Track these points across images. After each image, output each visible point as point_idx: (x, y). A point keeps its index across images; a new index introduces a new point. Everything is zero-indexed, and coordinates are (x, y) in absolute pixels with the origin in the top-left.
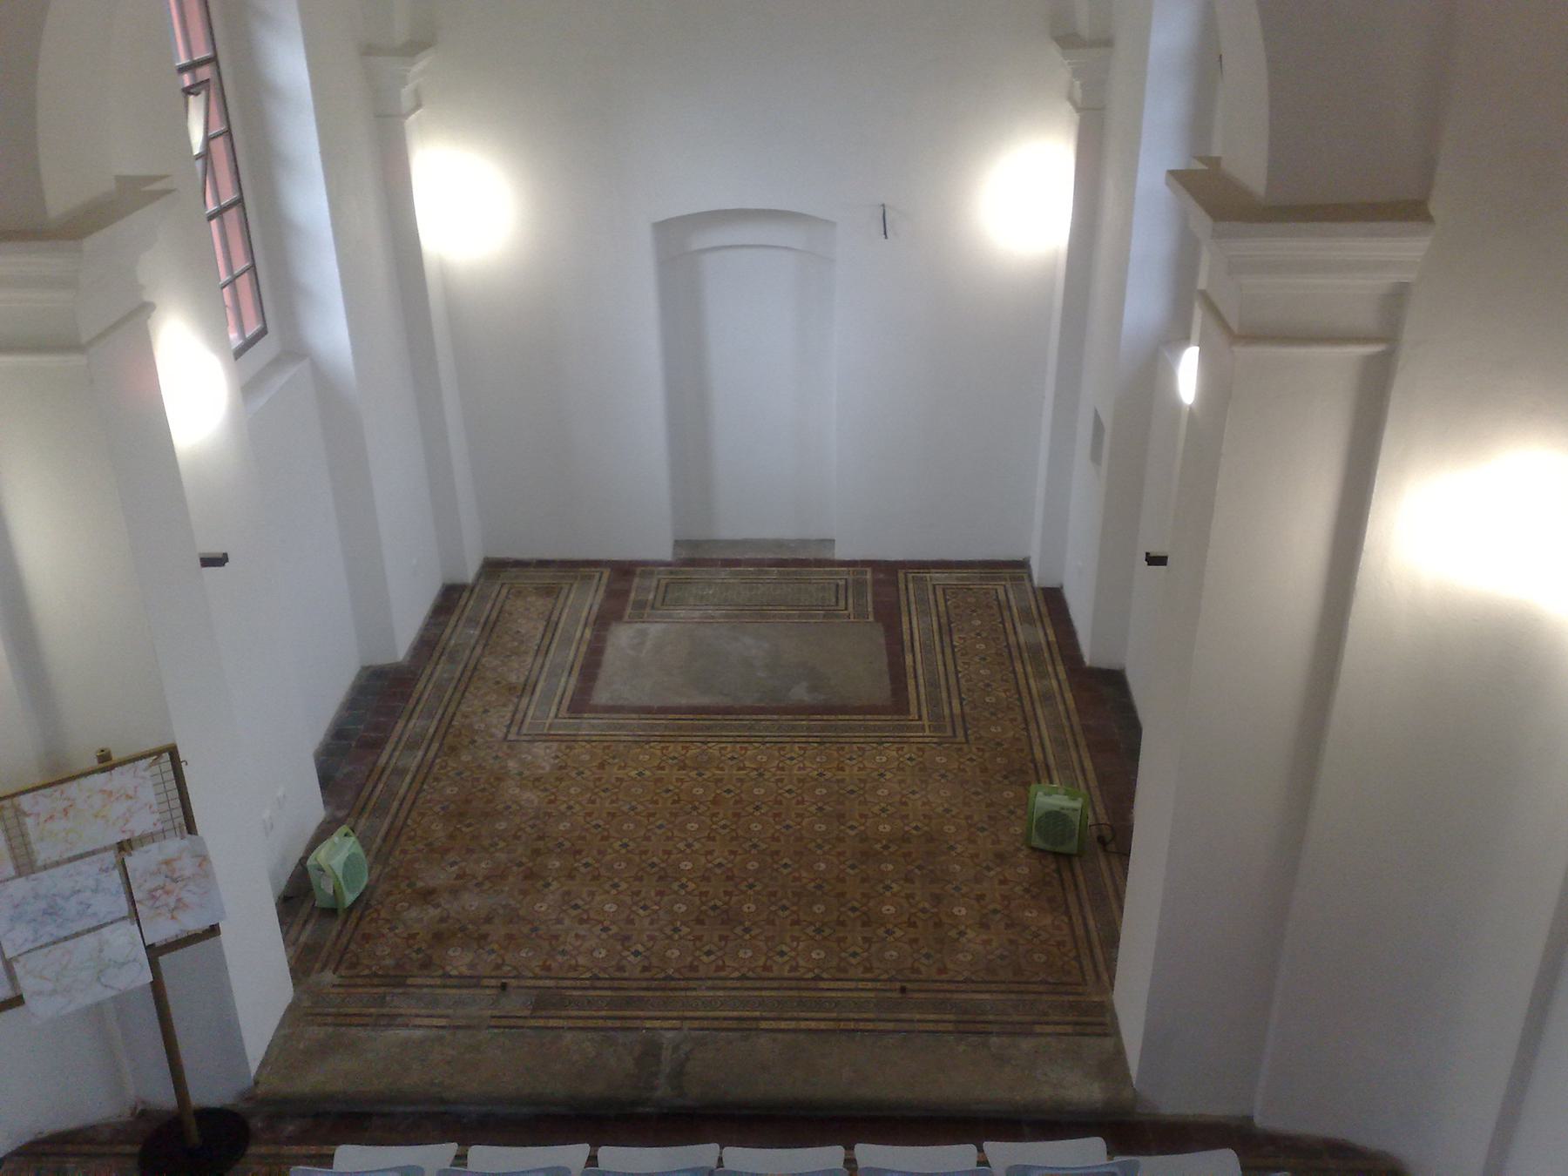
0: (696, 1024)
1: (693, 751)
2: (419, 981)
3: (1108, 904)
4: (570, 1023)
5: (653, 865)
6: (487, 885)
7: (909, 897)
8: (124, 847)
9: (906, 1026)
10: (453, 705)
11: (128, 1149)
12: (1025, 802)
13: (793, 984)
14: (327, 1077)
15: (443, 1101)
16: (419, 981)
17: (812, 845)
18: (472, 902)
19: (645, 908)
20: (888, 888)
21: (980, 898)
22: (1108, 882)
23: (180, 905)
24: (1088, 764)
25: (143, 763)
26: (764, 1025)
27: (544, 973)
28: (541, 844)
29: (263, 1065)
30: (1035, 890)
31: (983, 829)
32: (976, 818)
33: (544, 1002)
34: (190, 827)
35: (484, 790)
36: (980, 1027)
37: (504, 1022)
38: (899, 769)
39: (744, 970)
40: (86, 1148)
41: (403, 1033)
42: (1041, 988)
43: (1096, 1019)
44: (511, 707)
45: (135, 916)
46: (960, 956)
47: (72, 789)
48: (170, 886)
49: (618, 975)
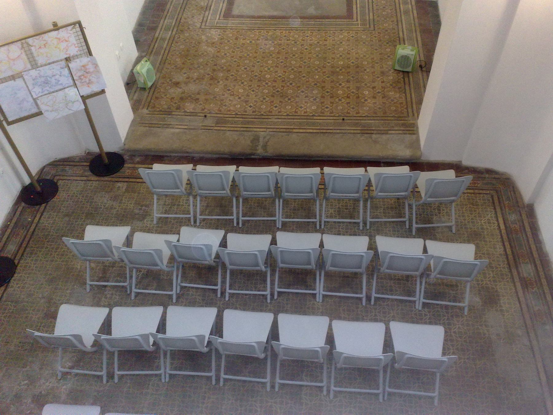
0: (271, 130)
1: (270, 33)
2: (177, 113)
3: (420, 90)
4: (229, 129)
5: (256, 76)
6: (197, 81)
7: (348, 87)
8: (68, 60)
9: (343, 131)
10: (181, 14)
11: (85, 164)
12: (394, 53)
13: (305, 117)
14: (149, 143)
15: (187, 153)
16: (177, 113)
17: (313, 70)
18: (193, 88)
19: (253, 91)
20: (340, 84)
21: (374, 88)
22: (421, 81)
23: (90, 83)
24: (419, 39)
25: (70, 28)
26: (295, 131)
27: (219, 112)
28: (215, 67)
29: (126, 139)
30: (394, 85)
31: (377, 63)
32: (375, 59)
33: (220, 122)
34: (90, 54)
35: (194, 47)
36: (369, 132)
37: (206, 128)
38: (348, 40)
39: (288, 113)
40: (72, 163)
41: (172, 130)
42: (392, 119)
43: (411, 129)
44: (202, 15)
45: (75, 85)
46: (365, 108)
47: (45, 36)
48: (86, 75)
49: (245, 113)
